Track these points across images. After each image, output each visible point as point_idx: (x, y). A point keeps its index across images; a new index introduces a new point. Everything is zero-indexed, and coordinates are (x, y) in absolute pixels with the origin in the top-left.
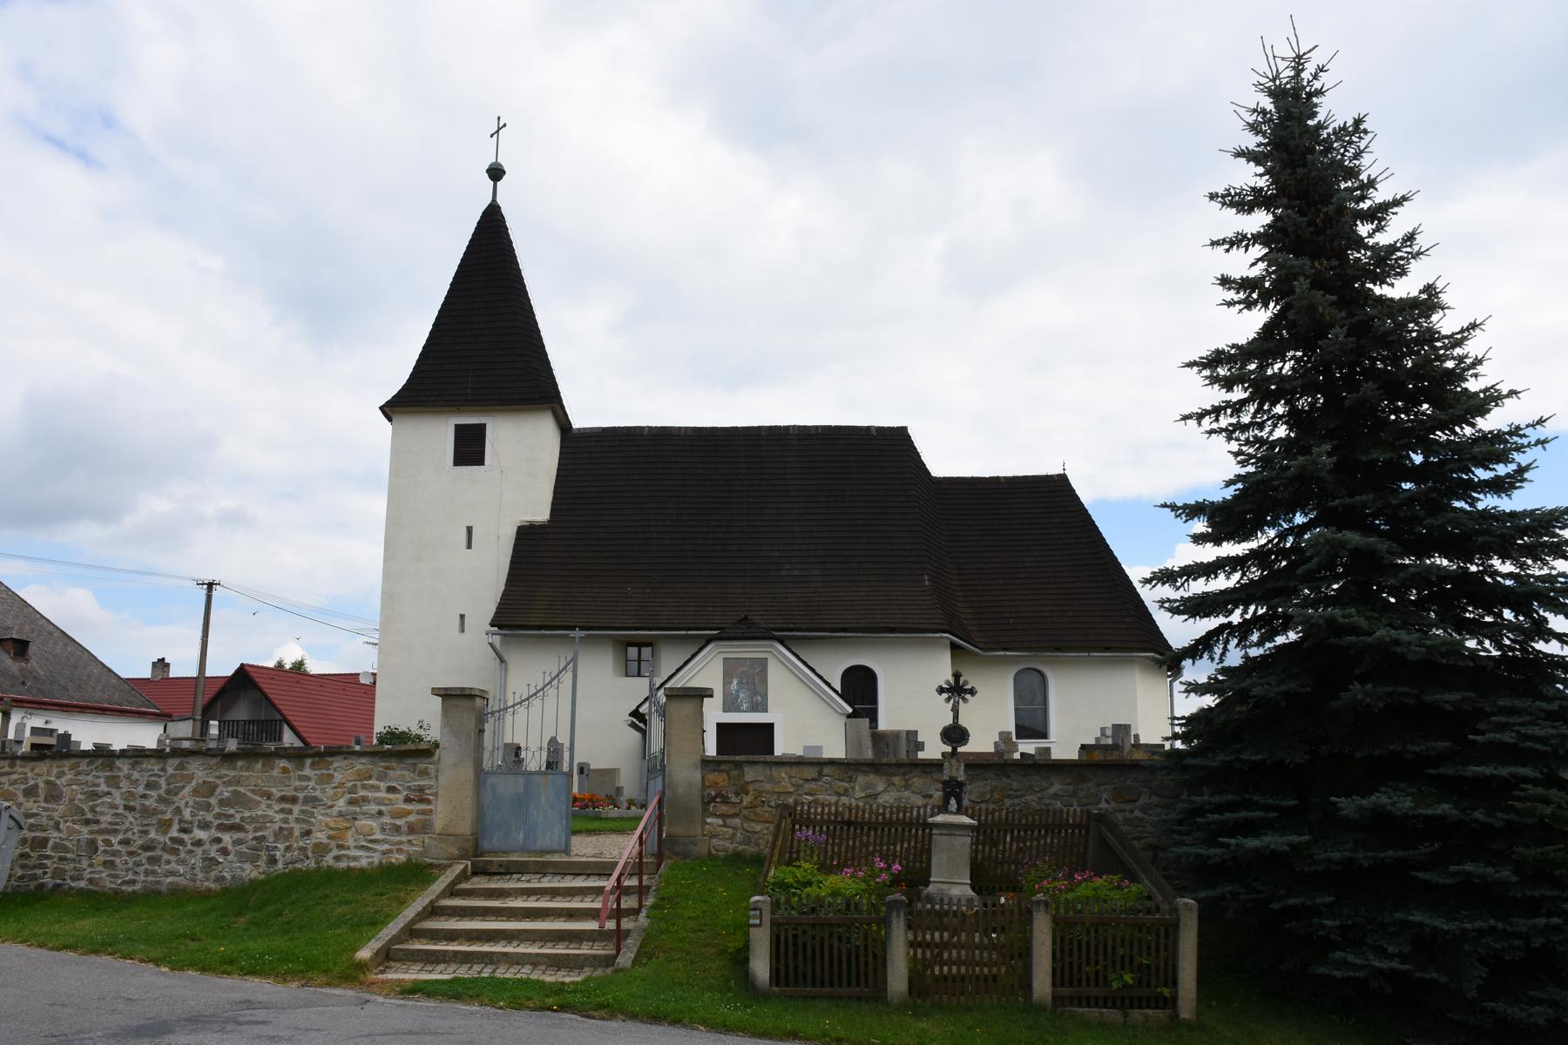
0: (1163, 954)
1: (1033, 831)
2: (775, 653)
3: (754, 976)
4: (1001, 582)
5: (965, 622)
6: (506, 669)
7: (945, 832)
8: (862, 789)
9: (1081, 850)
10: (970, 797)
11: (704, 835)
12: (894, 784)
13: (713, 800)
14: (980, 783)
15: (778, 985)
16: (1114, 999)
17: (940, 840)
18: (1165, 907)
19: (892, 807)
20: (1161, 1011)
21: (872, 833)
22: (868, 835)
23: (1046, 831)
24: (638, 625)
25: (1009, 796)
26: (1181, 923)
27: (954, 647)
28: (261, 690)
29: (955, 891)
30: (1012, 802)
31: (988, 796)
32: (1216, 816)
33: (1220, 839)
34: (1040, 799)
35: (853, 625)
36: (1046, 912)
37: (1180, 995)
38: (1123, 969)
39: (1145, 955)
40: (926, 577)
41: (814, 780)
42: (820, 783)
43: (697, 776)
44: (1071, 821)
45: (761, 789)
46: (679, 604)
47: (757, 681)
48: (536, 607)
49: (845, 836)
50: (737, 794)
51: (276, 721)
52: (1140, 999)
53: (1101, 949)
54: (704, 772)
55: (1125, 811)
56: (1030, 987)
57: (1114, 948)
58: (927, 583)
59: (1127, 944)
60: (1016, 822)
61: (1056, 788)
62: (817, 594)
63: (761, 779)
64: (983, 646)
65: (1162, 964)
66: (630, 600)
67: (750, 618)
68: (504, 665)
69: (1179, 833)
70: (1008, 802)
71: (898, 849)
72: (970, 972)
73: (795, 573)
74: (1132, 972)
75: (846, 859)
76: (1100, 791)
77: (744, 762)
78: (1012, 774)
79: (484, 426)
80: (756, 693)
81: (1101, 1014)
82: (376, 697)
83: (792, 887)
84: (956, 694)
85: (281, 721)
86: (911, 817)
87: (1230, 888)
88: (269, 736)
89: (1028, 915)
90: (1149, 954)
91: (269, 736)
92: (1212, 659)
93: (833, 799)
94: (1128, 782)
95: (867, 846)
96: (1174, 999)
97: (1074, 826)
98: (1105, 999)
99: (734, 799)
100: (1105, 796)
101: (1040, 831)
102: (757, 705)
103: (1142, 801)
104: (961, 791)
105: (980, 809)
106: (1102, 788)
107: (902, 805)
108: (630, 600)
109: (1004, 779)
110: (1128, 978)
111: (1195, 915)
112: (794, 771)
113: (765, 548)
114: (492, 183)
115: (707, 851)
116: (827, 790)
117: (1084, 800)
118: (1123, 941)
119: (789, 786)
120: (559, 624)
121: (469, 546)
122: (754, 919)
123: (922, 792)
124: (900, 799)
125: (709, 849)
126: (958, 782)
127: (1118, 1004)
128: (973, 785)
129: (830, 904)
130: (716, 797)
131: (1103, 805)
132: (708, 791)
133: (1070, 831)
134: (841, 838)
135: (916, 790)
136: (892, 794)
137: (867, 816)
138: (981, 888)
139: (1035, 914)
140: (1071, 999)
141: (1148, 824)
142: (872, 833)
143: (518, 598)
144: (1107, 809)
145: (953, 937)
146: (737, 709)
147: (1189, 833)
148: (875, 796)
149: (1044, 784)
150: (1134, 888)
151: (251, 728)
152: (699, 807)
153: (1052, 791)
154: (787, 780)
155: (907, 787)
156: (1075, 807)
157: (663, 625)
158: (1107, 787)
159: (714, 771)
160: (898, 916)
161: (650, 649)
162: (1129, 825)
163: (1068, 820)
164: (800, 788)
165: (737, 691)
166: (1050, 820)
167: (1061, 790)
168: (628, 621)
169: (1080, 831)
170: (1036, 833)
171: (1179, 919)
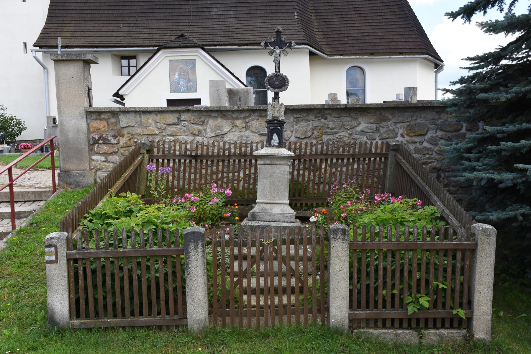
0: (459, 278)
1: (343, 160)
2: (200, 56)
3: (52, 310)
4: (340, 16)
5: (318, 40)
6: (47, 73)
7: (268, 162)
8: (212, 131)
9: (382, 173)
10: (296, 135)
11: (92, 169)
12: (237, 126)
13: (96, 142)
14: (304, 124)
15: (78, 316)
16: (410, 320)
17: (263, 169)
18: (461, 232)
19: (235, 143)
20: (455, 331)
21: (221, 164)
22: (218, 165)
23: (353, 159)
24: (125, 44)
25: (326, 133)
26: (479, 248)
27: (311, 54)
29: (276, 210)
30: (328, 137)
31: (310, 134)
32: (510, 144)
33: (516, 165)
34: (350, 135)
35: (252, 42)
36: (344, 239)
37: (475, 317)
38: (419, 292)
39: (441, 278)
40: (296, 14)
41: (174, 124)
42: (179, 127)
43: (83, 124)
44: (373, 151)
45: (133, 133)
46: (150, 32)
47: (190, 73)
49: (199, 166)
50: (115, 137)
52: (435, 320)
53: (398, 274)
54: (89, 121)
55: (416, 143)
56: (328, 310)
57: (410, 272)
58: (296, 17)
59: (423, 268)
60: (330, 153)
61: (363, 126)
62: (231, 25)
63: (133, 125)
64: (328, 53)
65: (458, 287)
67: (184, 34)
68: (46, 70)
69: (470, 160)
70: (325, 138)
71: (242, 175)
72: (269, 303)
73: (219, 13)
74: (427, 295)
75: (200, 184)
76: (397, 127)
77: (119, 111)
78: (329, 117)
81: (397, 335)
83: (109, 217)
84: (277, 47)
86: (246, 151)
87: (522, 211)
89: (326, 242)
90: (445, 278)
92: (502, 10)
93: (190, 138)
94: (419, 121)
95: (217, 173)
96: (470, 320)
97: (376, 155)
98: (401, 320)
99: (113, 141)
100: (401, 131)
101: (348, 159)
102: (191, 87)
103: (429, 135)
104: (282, 128)
105: (307, 143)
106: (398, 126)
107: (243, 142)
109: (323, 120)
110: (424, 301)
111: (493, 240)
112: (159, 117)
115: (93, 181)
116: (184, 132)
117: (385, 135)
118: (419, 265)
119: (155, 129)
120: (76, 44)
122: (50, 255)
123: (259, 132)
124: (241, 137)
125: (95, 179)
126: (279, 121)
127: (414, 325)
128: (298, 126)
129: (137, 234)
130: (98, 140)
131: (399, 138)
132: (93, 135)
133: (372, 159)
134: (196, 168)
135: (254, 130)
136: (236, 133)
137: (216, 151)
138: (296, 204)
139: (332, 242)
140: (367, 320)
141: (434, 153)
142: (221, 164)
143: (53, 30)
144: (402, 141)
145: (252, 266)
146: (179, 91)
147: (478, 159)
148: (223, 135)
149: (353, 123)
150: (429, 209)
152: (86, 147)
153: (359, 128)
154: (153, 124)
155: (247, 128)
156: (377, 140)
157: (139, 44)
158: (402, 124)
159: (96, 119)
160: (195, 248)
161: (135, 60)
162: (419, 154)
163: (371, 150)
164: (163, 131)
165: (178, 80)
166: (357, 150)
167: (367, 127)
169: (381, 159)
170: (345, 161)
171: (476, 245)
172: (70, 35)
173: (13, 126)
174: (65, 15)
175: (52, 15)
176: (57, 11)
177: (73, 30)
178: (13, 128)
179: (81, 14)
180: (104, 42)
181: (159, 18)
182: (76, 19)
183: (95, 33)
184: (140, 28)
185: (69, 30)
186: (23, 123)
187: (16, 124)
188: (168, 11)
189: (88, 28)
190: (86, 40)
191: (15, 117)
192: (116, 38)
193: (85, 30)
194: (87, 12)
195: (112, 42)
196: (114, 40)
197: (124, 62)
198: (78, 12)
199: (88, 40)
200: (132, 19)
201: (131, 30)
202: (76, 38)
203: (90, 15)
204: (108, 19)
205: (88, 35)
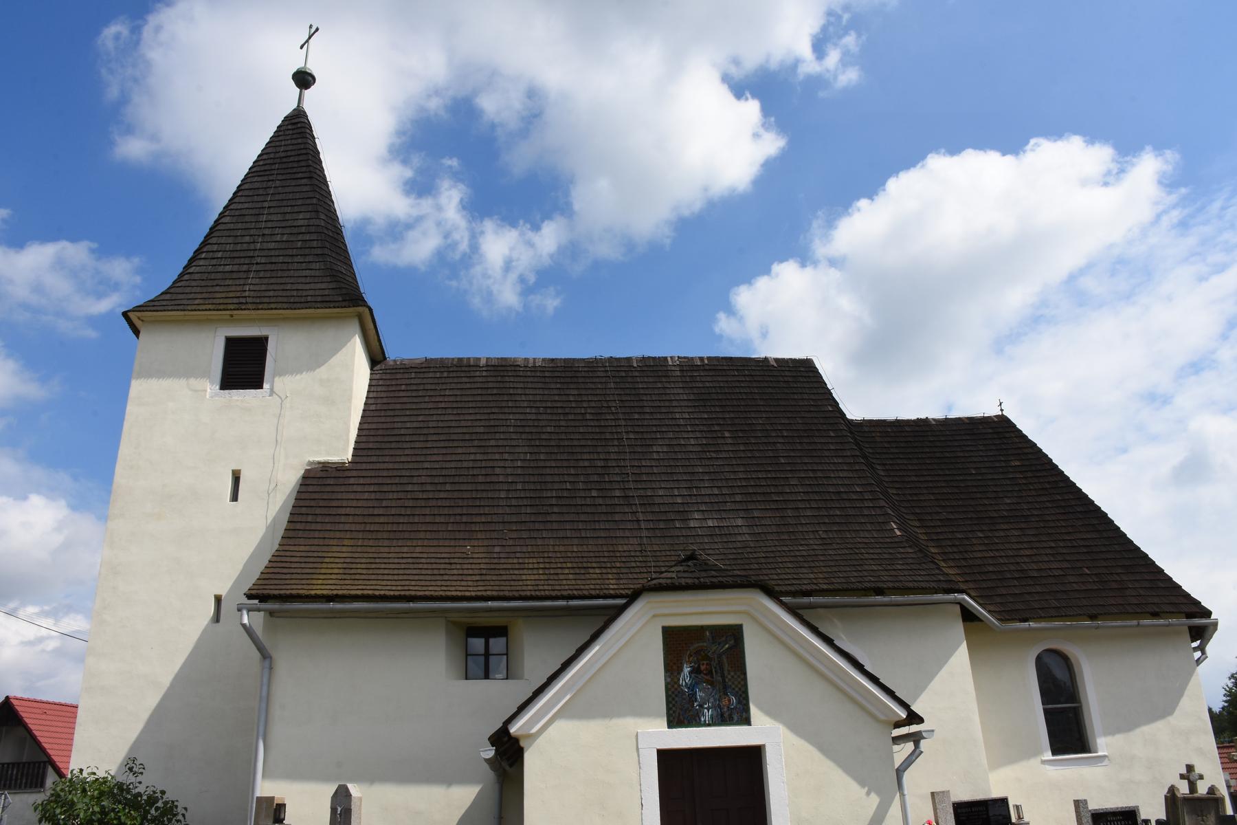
6: (271, 668)
47: (726, 667)
48: (323, 571)
66: (471, 561)
68: (267, 663)
73: (710, 523)
79: (261, 343)
80: (725, 690)
85: (45, 762)
88: (29, 781)
91: (29, 781)
113: (661, 492)
114: (299, 90)
121: (235, 497)
151: (15, 772)
165: (692, 688)
172: (341, 571)
176: (310, 519)
188: (583, 517)
193: (377, 561)
199: (389, 583)
203: (389, 528)
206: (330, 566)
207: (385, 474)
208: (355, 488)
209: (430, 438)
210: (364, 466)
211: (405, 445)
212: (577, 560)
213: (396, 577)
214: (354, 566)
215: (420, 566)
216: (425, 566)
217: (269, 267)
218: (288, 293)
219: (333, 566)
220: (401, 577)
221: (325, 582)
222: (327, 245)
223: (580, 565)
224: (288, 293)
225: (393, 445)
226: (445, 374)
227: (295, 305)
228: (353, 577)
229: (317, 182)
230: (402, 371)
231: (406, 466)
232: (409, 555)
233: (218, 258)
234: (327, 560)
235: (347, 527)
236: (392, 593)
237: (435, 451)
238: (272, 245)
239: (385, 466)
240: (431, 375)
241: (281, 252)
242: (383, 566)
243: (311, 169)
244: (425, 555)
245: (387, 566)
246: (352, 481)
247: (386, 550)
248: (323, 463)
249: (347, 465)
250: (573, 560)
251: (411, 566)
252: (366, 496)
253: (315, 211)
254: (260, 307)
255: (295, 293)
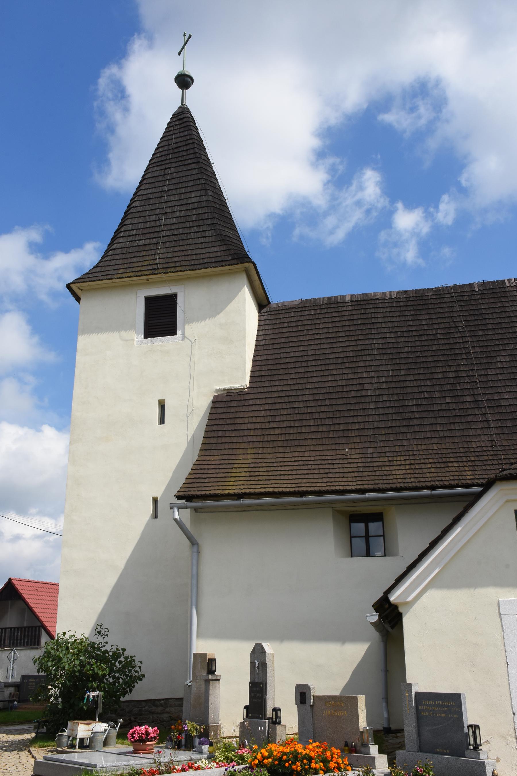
6: (198, 552)
28: (27, 604)
51: (36, 627)
66: (350, 461)
68: (195, 547)
82: (60, 595)
85: (39, 627)
108: (350, 461)
113: (506, 396)
114: (181, 90)
120: (262, 490)
121: (162, 421)
168: (351, 484)
172: (247, 474)
173: (118, 671)
174: (235, 440)
175: (212, 440)
176: (220, 434)
177: (252, 465)
178: (117, 675)
179: (266, 437)
180: (318, 485)
181: (422, 435)
182: (256, 445)
183: (295, 468)
184: (388, 454)
185: (243, 466)
186: (137, 663)
187: (124, 667)
188: (440, 421)
189: (281, 460)
190: (282, 482)
191: (124, 650)
192: (341, 475)
194: (277, 431)
195: (337, 484)
196: (340, 479)
197: (359, 527)
198: (259, 432)
200: (367, 439)
201: (370, 460)
202: (260, 478)
203: (282, 438)
204: (319, 442)
205: (282, 473)
206: (238, 470)
207: (276, 395)
208: (254, 408)
209: (310, 364)
210: (259, 390)
211: (290, 371)
212: (437, 456)
213: (290, 477)
214: (257, 469)
215: (309, 467)
216: (313, 467)
217: (173, 238)
218: (189, 258)
219: (241, 470)
220: (294, 477)
221: (235, 483)
222: (216, 216)
223: (440, 460)
224: (189, 258)
225: (281, 372)
226: (318, 311)
227: (195, 267)
228: (257, 478)
229: (203, 166)
230: (283, 312)
231: (292, 387)
232: (299, 459)
233: (133, 235)
234: (236, 466)
235: (250, 439)
236: (288, 490)
237: (315, 374)
238: (174, 221)
239: (276, 389)
240: (307, 313)
241: (181, 226)
242: (280, 468)
243: (198, 155)
244: (312, 458)
245: (283, 468)
246: (251, 402)
247: (281, 455)
248: (228, 390)
249: (246, 390)
250: (433, 456)
251: (302, 467)
252: (263, 413)
253: (204, 189)
254: (169, 271)
255: (194, 257)
